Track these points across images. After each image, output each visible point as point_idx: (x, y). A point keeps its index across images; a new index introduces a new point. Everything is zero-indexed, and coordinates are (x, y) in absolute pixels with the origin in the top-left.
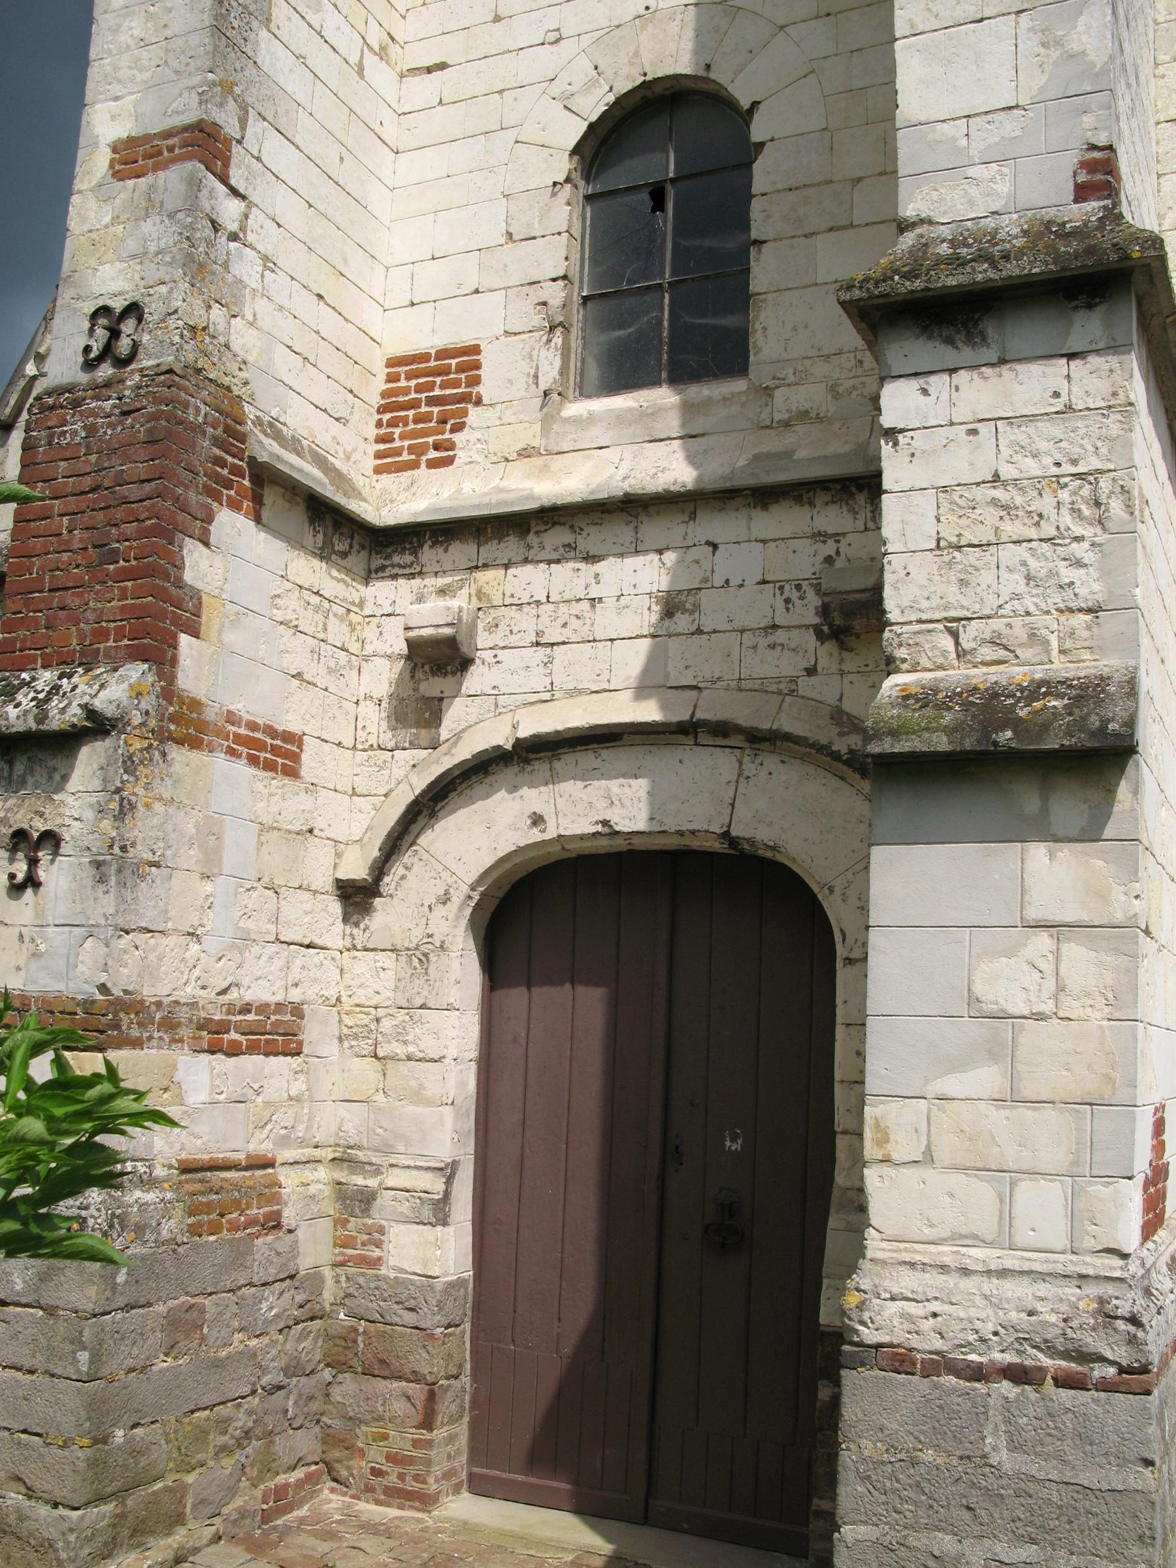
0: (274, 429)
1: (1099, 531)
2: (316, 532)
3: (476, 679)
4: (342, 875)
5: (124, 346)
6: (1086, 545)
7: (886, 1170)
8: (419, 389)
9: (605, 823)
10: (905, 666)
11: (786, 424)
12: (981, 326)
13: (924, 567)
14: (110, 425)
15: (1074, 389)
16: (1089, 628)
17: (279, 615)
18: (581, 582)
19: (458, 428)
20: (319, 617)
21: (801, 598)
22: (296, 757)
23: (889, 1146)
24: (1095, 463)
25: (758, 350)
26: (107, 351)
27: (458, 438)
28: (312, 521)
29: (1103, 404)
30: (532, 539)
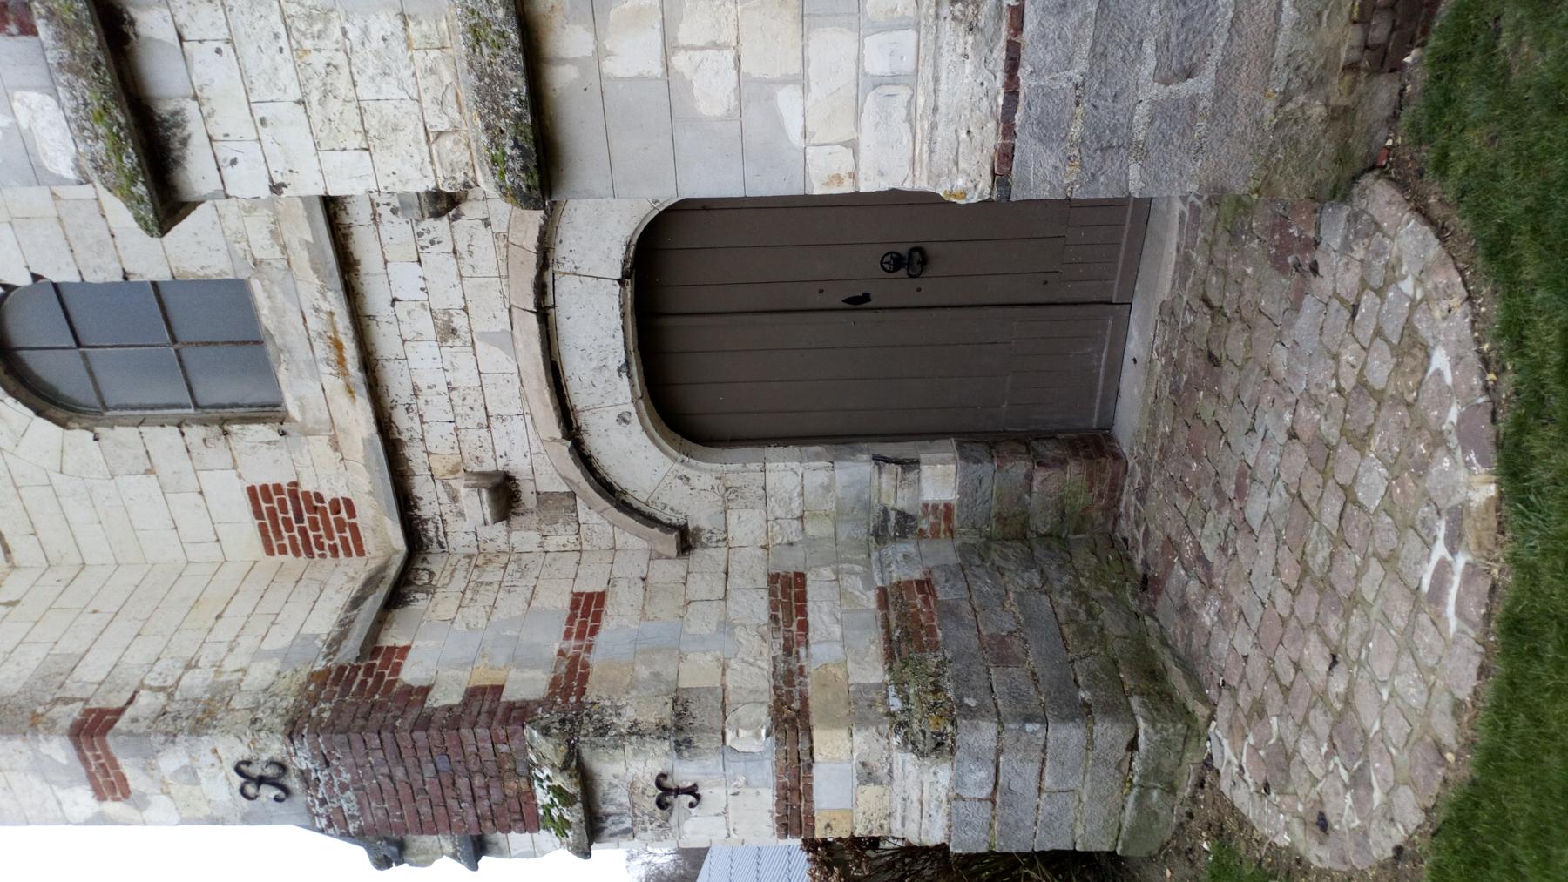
0: (335, 643)
1: (333, 15)
2: (415, 599)
3: (518, 465)
4: (673, 551)
5: (270, 772)
6: (348, 26)
7: (861, 176)
8: (290, 529)
9: (619, 370)
10: (471, 174)
11: (284, 248)
12: (166, 115)
13: (387, 162)
14: (339, 773)
15: (212, 36)
16: (419, 23)
17: (482, 622)
18: (436, 399)
19: (319, 498)
20: (482, 589)
21: (429, 232)
22: (590, 596)
23: (843, 174)
24: (275, 18)
25: (222, 271)
26: (274, 783)
27: (327, 498)
28: (406, 604)
29: (221, 11)
30: (405, 437)
